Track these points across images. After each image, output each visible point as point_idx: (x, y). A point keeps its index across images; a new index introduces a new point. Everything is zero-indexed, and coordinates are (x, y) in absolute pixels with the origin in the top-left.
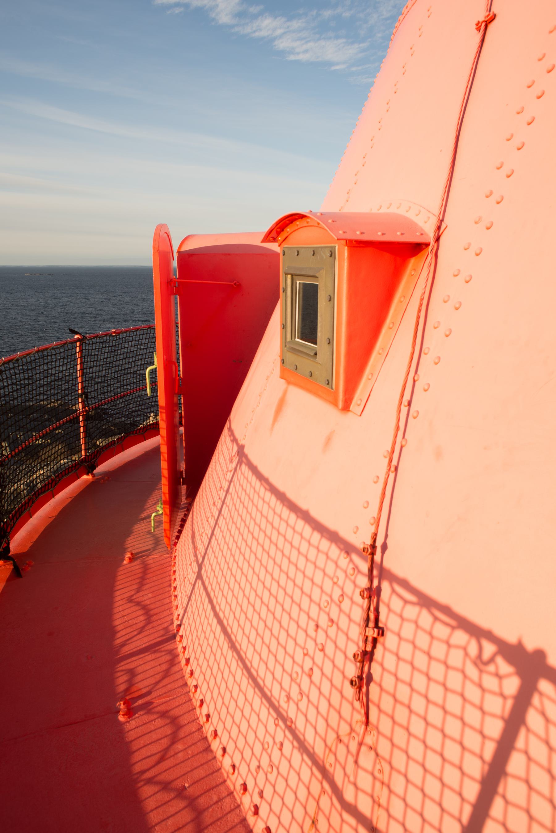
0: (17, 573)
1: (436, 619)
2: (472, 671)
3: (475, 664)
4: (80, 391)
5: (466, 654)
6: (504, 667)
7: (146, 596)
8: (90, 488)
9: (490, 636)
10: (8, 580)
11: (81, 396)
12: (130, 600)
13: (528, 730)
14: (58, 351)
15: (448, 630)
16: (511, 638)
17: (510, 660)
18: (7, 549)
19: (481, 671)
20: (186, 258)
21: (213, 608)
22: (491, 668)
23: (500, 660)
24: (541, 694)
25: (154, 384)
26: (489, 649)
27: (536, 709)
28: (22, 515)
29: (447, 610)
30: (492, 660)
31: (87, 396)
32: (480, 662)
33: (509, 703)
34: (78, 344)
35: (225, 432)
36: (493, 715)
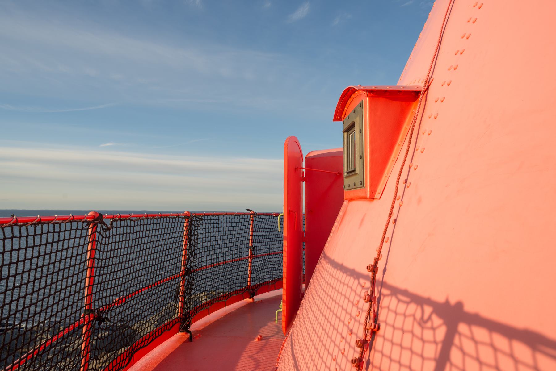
0: (191, 339)
1: (399, 300)
2: (417, 330)
3: (419, 324)
4: (250, 245)
5: (415, 319)
6: (437, 321)
7: (262, 357)
8: (249, 305)
9: (428, 301)
10: (184, 342)
11: (250, 247)
12: (250, 357)
13: (452, 364)
14: (238, 217)
15: (404, 306)
16: (440, 298)
17: (440, 315)
18: (189, 326)
19: (423, 328)
20: (311, 161)
21: (292, 351)
22: (429, 324)
23: (434, 318)
24: (460, 334)
25: (282, 224)
26: (428, 310)
27: (457, 346)
28: (203, 310)
29: (405, 293)
30: (430, 318)
31: (254, 248)
32: (422, 323)
33: (440, 346)
34: (251, 216)
35: (322, 255)
36: (429, 359)
